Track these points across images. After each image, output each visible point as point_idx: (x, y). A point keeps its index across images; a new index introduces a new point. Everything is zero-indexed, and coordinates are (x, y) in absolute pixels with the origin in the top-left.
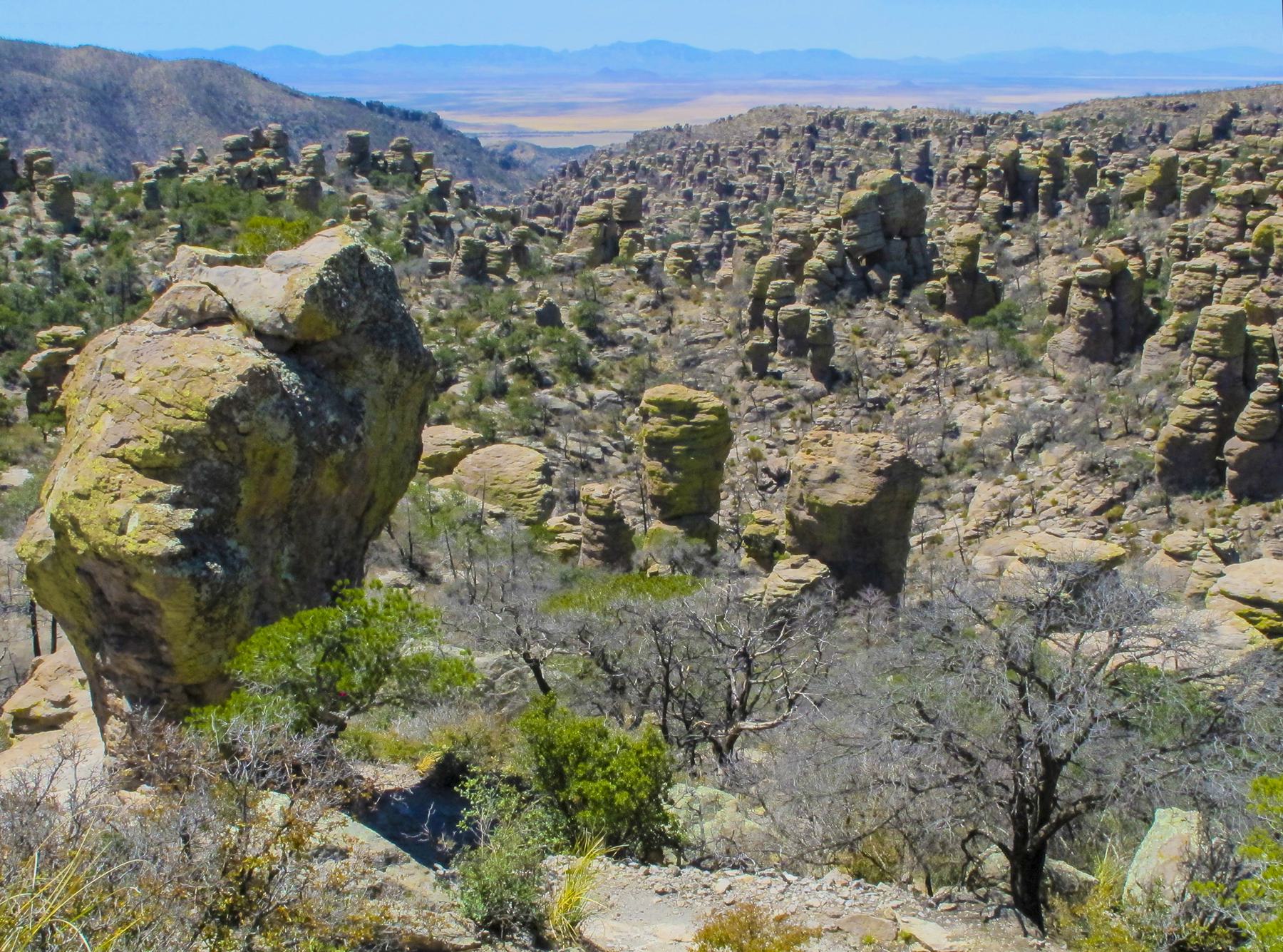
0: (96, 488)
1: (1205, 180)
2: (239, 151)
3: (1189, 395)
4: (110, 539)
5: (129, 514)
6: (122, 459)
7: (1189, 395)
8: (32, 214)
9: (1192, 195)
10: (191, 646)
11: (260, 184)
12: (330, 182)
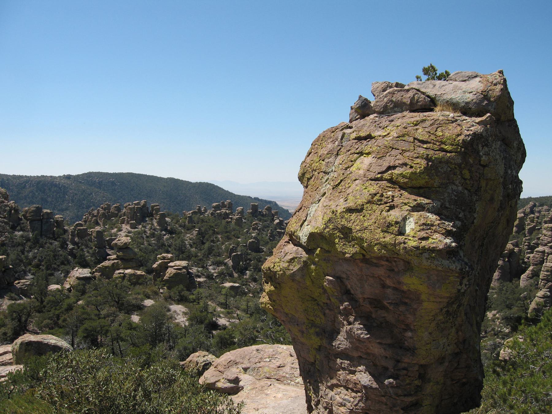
0: (369, 202)
1: (534, 224)
2: (217, 208)
3: (540, 293)
4: (388, 239)
5: (405, 219)
6: (390, 181)
7: (540, 293)
8: (153, 224)
9: (529, 229)
10: (430, 333)
11: (224, 219)
12: (245, 219)
